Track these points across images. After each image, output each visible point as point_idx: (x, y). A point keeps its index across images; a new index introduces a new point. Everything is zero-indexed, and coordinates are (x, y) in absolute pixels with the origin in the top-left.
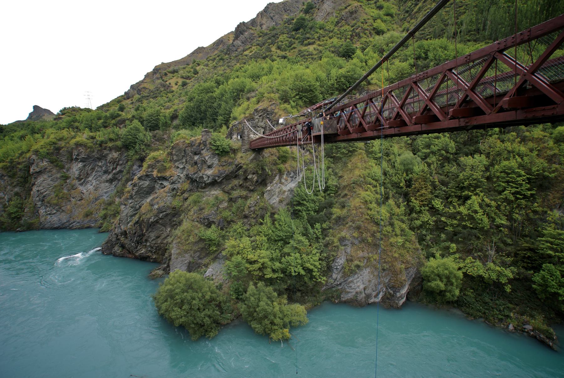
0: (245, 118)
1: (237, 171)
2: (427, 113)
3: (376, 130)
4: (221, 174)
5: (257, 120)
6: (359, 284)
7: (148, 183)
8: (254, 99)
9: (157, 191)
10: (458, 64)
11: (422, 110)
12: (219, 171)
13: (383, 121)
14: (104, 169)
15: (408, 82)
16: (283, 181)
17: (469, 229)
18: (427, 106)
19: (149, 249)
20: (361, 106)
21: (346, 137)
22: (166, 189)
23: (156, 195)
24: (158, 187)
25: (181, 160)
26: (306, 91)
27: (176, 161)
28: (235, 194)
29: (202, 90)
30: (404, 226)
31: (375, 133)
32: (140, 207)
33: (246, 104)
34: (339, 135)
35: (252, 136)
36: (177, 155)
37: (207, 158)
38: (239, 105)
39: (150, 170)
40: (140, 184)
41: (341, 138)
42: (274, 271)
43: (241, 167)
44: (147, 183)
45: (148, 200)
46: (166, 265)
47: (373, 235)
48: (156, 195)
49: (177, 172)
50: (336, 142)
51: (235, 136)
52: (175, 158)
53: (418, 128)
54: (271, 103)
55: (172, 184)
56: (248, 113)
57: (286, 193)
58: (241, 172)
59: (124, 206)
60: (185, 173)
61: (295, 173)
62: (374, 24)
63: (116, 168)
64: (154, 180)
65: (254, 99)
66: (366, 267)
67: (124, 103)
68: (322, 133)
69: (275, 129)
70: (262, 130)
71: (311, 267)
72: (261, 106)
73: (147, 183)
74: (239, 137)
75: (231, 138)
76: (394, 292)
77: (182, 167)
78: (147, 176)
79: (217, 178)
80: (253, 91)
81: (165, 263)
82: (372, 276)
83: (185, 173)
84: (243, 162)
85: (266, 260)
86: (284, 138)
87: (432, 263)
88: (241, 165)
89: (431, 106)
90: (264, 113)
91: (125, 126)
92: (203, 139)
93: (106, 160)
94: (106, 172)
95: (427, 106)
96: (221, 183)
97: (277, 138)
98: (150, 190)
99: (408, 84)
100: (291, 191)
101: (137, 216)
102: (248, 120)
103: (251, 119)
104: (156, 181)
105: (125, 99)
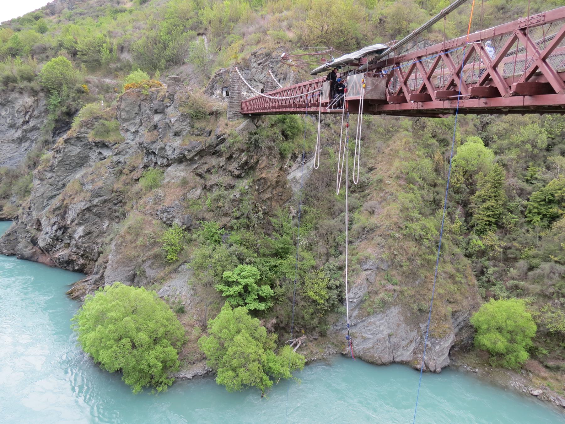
0: (237, 64)
1: (217, 145)
2: (535, 79)
4: (194, 147)
5: (254, 70)
6: (382, 328)
7: (78, 150)
9: (93, 164)
10: (428, 53)
11: (528, 74)
12: (190, 142)
13: (460, 88)
14: (8, 120)
15: (511, 29)
17: (553, 263)
18: (537, 68)
19: (74, 250)
20: (430, 62)
21: (397, 107)
22: (107, 162)
23: (91, 169)
24: (94, 157)
25: (132, 119)
27: (125, 120)
28: (213, 179)
29: (172, 14)
30: (457, 251)
31: (447, 104)
32: (64, 185)
34: (387, 103)
35: (244, 93)
36: (127, 112)
37: (173, 120)
39: (82, 130)
40: (67, 150)
41: (391, 107)
42: (261, 299)
43: (223, 140)
44: (76, 150)
45: (78, 175)
46: (98, 276)
47: (411, 260)
48: (90, 170)
49: (132, 138)
51: (218, 92)
52: (124, 115)
53: (518, 101)
54: (277, 46)
55: (116, 154)
56: (241, 56)
58: (222, 147)
59: (39, 182)
60: (137, 139)
61: (304, 156)
63: (28, 122)
64: (88, 146)
66: (394, 304)
67: (45, 20)
69: (281, 86)
70: (261, 86)
71: (315, 297)
73: (76, 150)
74: (224, 93)
75: (212, 94)
76: (432, 343)
77: (133, 130)
78: (78, 138)
79: (186, 153)
81: (97, 273)
82: (402, 318)
83: (137, 139)
84: (228, 131)
85: (251, 281)
86: (298, 100)
87: (492, 306)
88: (226, 136)
89: (543, 69)
90: (266, 60)
91: (47, 57)
92: (170, 91)
93: (13, 107)
94: (12, 126)
95: (537, 68)
96: (192, 160)
97: (282, 100)
98: (83, 161)
99: (511, 32)
101: (60, 197)
102: (241, 69)
103: (245, 66)
104: (91, 148)
105: (47, 14)
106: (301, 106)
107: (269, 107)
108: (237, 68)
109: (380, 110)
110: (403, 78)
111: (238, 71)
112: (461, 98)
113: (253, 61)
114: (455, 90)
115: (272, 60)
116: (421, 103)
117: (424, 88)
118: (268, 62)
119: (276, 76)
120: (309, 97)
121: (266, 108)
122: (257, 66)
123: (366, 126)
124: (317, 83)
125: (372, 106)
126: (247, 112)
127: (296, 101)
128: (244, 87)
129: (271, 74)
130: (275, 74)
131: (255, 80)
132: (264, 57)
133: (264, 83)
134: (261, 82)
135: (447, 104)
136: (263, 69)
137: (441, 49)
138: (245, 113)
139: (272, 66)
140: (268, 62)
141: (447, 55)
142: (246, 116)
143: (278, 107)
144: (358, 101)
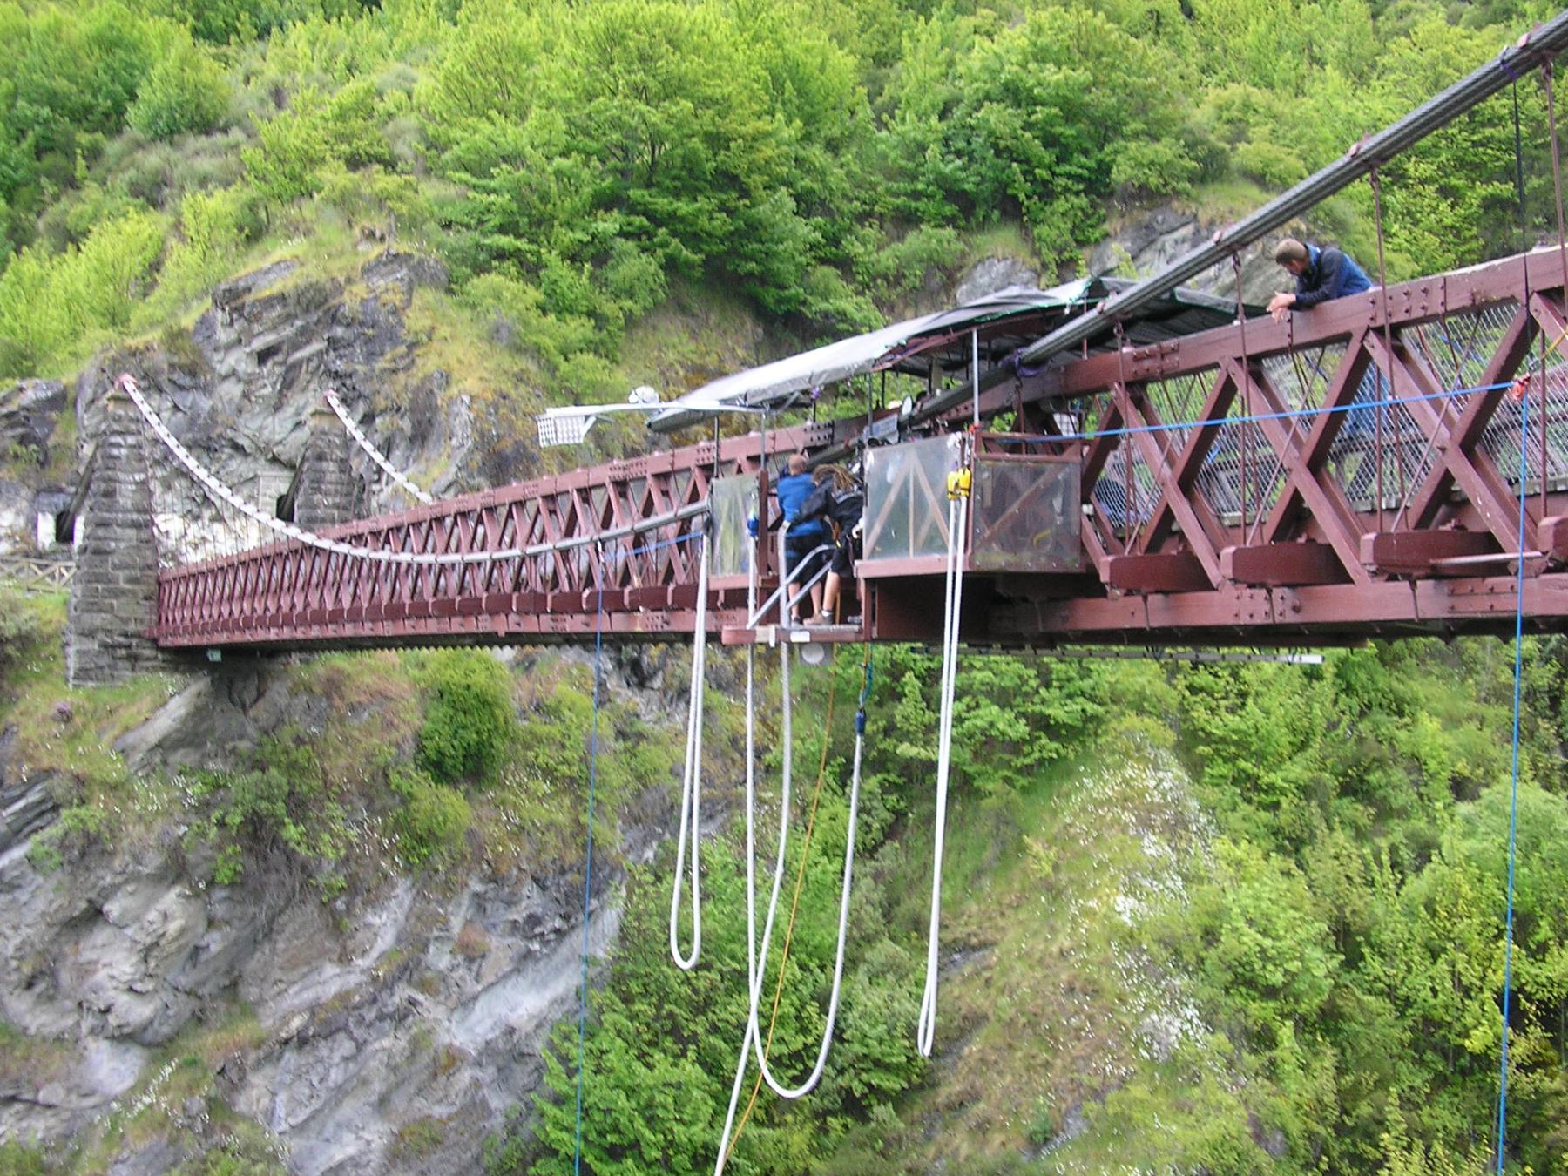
3: (1436, 574)
5: (233, 390)
8: (221, 203)
16: (440, 958)
21: (1156, 612)
26: (689, 180)
33: (121, 235)
34: (1099, 591)
35: (170, 524)
38: (70, 238)
41: (1118, 611)
50: (1051, 641)
57: (465, 1076)
62: (399, 67)
65: (221, 203)
68: (953, 562)
70: (276, 484)
72: (283, 265)
80: (206, 126)
90: (305, 335)
100: (508, 1053)
102: (151, 384)
106: (570, 604)
107: (274, 618)
108: (129, 382)
109: (1058, 626)
110: (1170, 460)
111: (138, 397)
112: (1501, 569)
113: (223, 336)
114: (1460, 527)
115: (339, 331)
116: (1286, 591)
117: (1296, 516)
118: (317, 346)
119: (367, 420)
120: (620, 555)
121: (336, 617)
122: (247, 367)
123: (909, 904)
124: (662, 477)
125: (1008, 609)
126: (198, 640)
127: (535, 577)
128: (168, 487)
129: (341, 411)
130: (361, 408)
131: (238, 448)
132: (289, 318)
133: (290, 466)
134: (275, 460)
135: (1429, 601)
136: (288, 384)
137: (1365, 322)
138: (184, 641)
139: (340, 365)
140: (317, 346)
141: (1400, 353)
142: (186, 659)
143: (355, 615)
144: (936, 582)
